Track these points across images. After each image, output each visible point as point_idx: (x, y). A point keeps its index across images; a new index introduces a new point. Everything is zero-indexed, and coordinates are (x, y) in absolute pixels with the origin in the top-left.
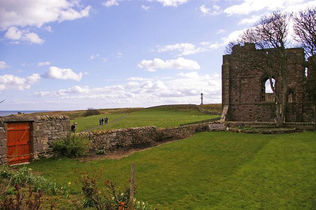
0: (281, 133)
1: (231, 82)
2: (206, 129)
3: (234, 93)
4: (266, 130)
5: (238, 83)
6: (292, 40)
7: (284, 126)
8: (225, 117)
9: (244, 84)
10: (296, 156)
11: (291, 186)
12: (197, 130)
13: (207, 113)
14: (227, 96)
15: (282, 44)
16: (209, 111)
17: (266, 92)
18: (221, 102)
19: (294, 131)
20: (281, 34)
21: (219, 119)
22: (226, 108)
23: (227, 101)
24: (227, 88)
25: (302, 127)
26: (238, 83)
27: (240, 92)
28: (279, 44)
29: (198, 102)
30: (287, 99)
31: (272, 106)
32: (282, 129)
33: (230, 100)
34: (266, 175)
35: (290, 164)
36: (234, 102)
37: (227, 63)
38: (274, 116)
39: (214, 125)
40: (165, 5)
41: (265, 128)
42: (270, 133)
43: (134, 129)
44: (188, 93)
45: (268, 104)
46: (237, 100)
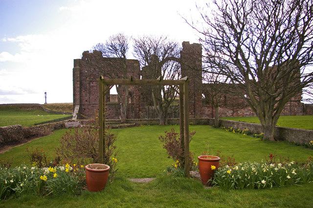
0: (125, 127)
1: (81, 84)
2: (63, 126)
3: (84, 94)
4: (114, 126)
5: (88, 85)
6: (130, 55)
7: (127, 122)
8: (77, 116)
9: (93, 86)
10: (138, 140)
11: (138, 154)
12: (56, 128)
13: (52, 113)
14: (78, 97)
15: (125, 56)
16: (54, 110)
17: (110, 94)
18: (72, 102)
19: (134, 126)
20: (124, 51)
21: (72, 117)
22: (77, 108)
23: (78, 101)
24: (78, 89)
25: (139, 122)
26: (88, 85)
27: (90, 93)
28: (123, 57)
29: (41, 102)
30: (128, 101)
31: (117, 107)
32: (126, 124)
33: (81, 101)
34: (124, 151)
35: (136, 145)
36: (84, 102)
37: (78, 67)
38: (118, 114)
39: (70, 123)
40: (90, 52)
41: (113, 124)
42: (117, 128)
43: (3, 127)
44: (30, 92)
45: (112, 104)
46: (86, 101)
